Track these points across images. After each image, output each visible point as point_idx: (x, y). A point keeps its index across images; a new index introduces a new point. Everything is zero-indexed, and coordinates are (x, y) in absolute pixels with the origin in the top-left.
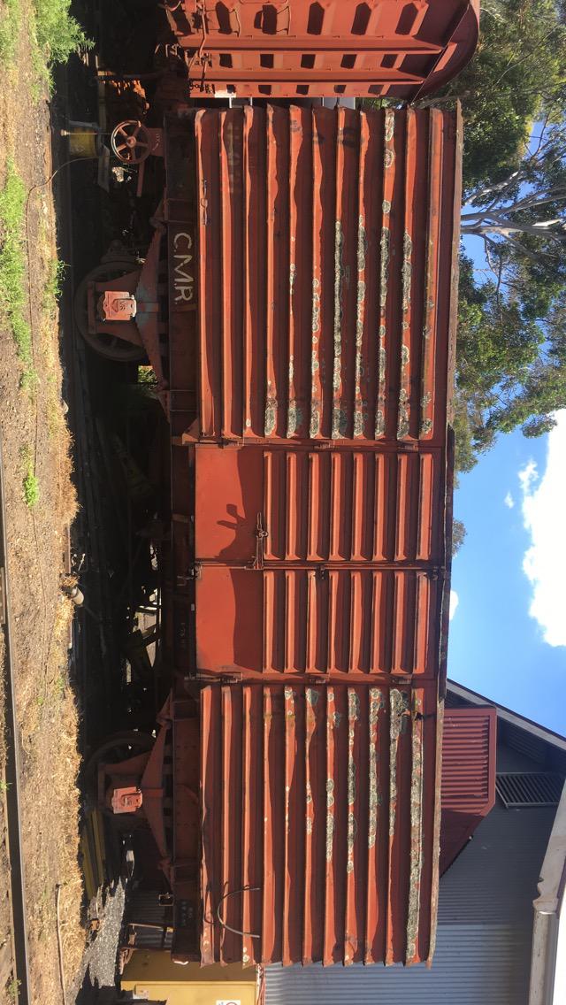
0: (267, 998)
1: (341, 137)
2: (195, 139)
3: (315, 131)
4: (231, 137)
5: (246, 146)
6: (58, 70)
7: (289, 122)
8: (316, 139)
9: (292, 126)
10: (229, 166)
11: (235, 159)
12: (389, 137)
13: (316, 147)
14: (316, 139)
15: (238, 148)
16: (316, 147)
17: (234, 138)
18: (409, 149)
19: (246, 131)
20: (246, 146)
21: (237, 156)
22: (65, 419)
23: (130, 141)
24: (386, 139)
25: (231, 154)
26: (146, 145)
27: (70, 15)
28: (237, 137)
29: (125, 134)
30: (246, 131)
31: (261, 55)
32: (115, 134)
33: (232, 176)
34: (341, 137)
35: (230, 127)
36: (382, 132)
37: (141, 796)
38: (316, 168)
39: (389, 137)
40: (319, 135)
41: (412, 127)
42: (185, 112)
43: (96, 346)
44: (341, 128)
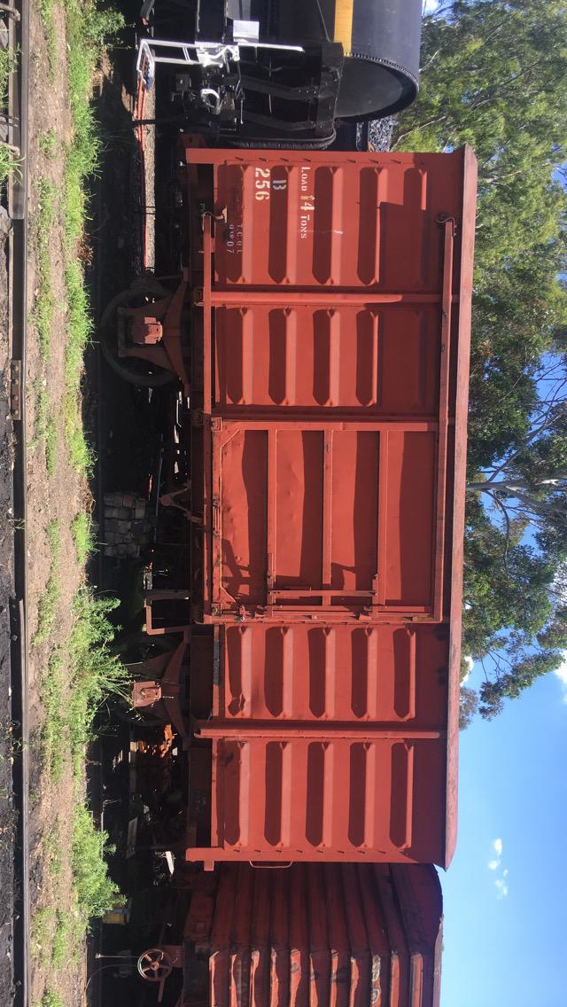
0: (314, 832)
1: (334, 977)
2: (209, 973)
3: (312, 970)
4: (240, 970)
5: (252, 982)
6: (94, 921)
7: (289, 966)
8: (312, 977)
9: (293, 969)
10: (237, 995)
11: (242, 987)
12: (376, 978)
13: (313, 984)
14: (312, 977)
15: (246, 977)
16: (313, 984)
17: (242, 972)
18: (392, 988)
19: (253, 971)
20: (252, 982)
21: (246, 985)
22: (84, 187)
23: (153, 966)
24: (373, 980)
25: (239, 985)
26: (167, 967)
27: (107, 876)
28: (245, 970)
29: (150, 959)
30: (253, 971)
31: (305, 433)
32: (140, 960)
33: (240, 1002)
34: (334, 977)
35: (240, 963)
36: (370, 976)
37: (160, 690)
38: (312, 1001)
39: (376, 978)
40: (315, 973)
41: (396, 969)
42: (201, 949)
43: (125, 373)
44: (334, 971)
